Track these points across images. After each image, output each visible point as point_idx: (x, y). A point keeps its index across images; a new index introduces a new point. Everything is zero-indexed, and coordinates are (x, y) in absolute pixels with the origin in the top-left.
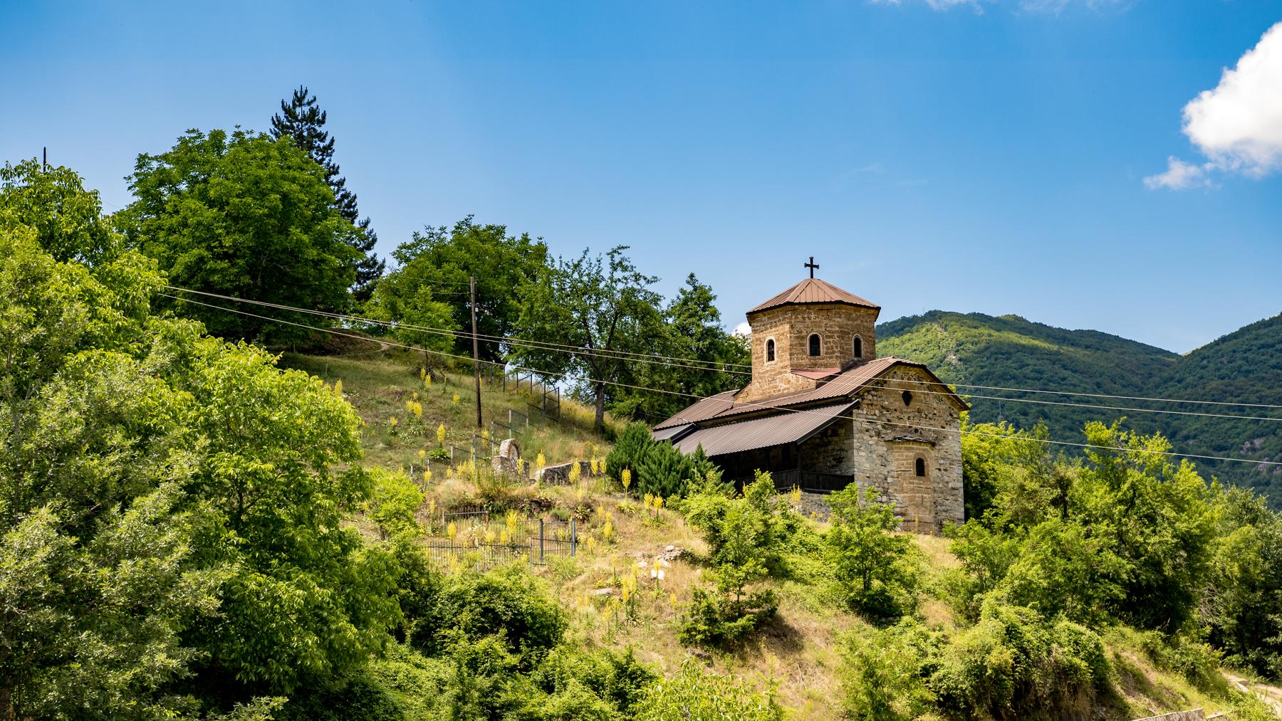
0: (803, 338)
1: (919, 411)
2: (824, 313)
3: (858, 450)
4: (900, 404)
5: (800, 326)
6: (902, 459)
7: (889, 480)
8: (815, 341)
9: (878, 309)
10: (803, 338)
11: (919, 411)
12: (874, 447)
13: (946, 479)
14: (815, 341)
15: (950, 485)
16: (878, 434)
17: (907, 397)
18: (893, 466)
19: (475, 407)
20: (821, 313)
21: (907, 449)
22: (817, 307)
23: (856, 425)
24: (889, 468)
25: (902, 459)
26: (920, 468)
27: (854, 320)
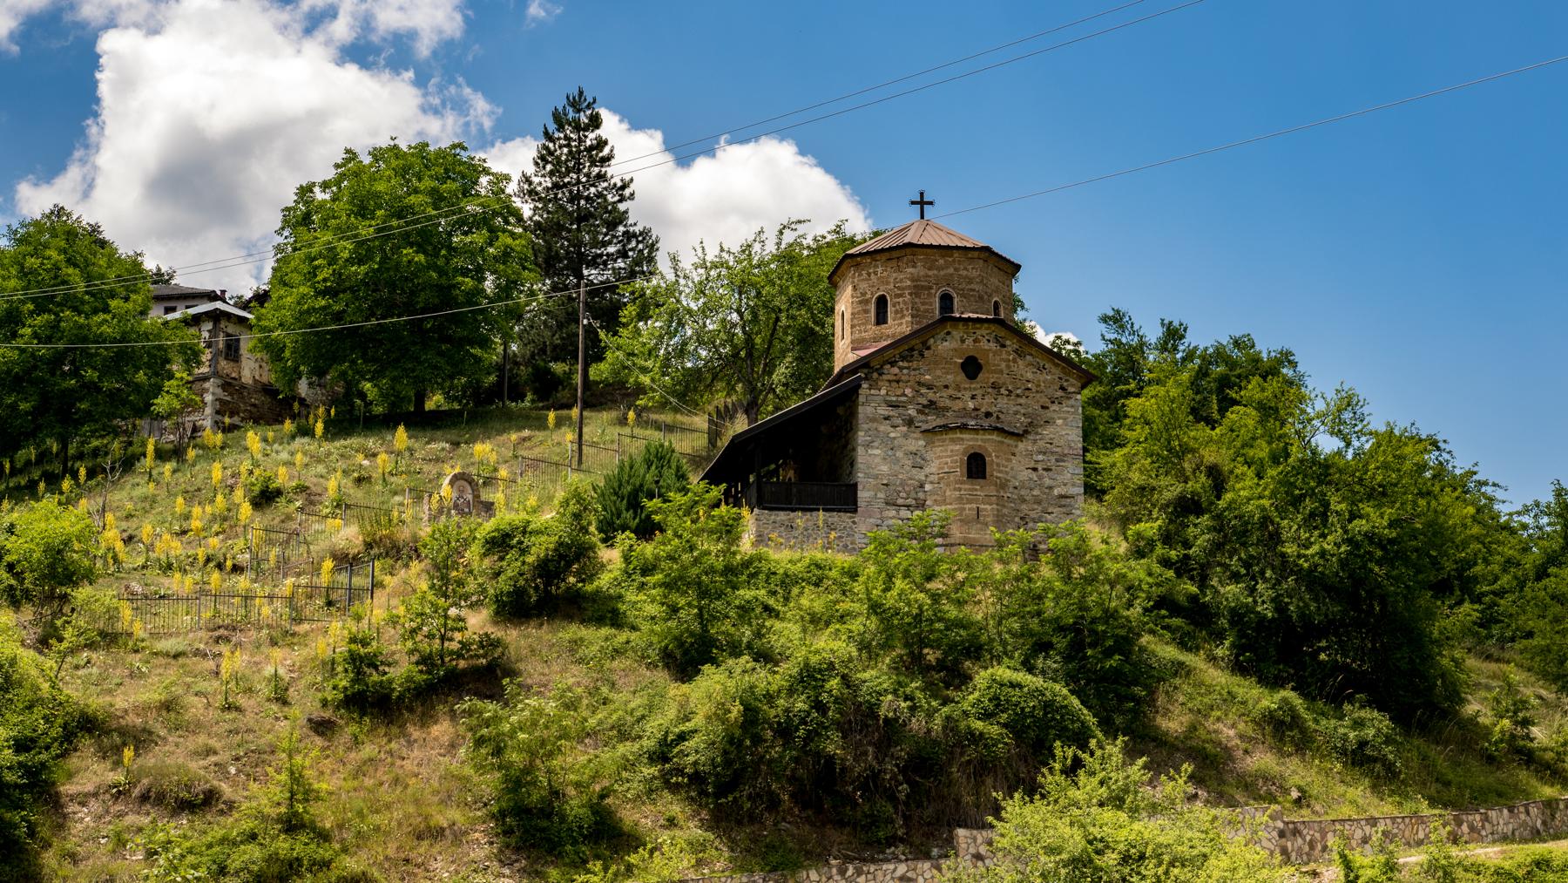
0: (867, 302)
1: (995, 386)
2: (894, 263)
3: (868, 445)
4: (956, 377)
5: (863, 286)
6: (946, 457)
7: (928, 487)
8: (882, 303)
9: (1018, 267)
10: (867, 302)
11: (995, 386)
12: (901, 441)
13: (1047, 482)
14: (882, 303)
15: (1056, 492)
16: (910, 422)
17: (972, 367)
18: (932, 468)
19: (585, 437)
20: (890, 264)
21: (952, 440)
22: (884, 256)
23: (864, 411)
24: (927, 470)
25: (946, 457)
26: (976, 466)
27: (939, 269)
